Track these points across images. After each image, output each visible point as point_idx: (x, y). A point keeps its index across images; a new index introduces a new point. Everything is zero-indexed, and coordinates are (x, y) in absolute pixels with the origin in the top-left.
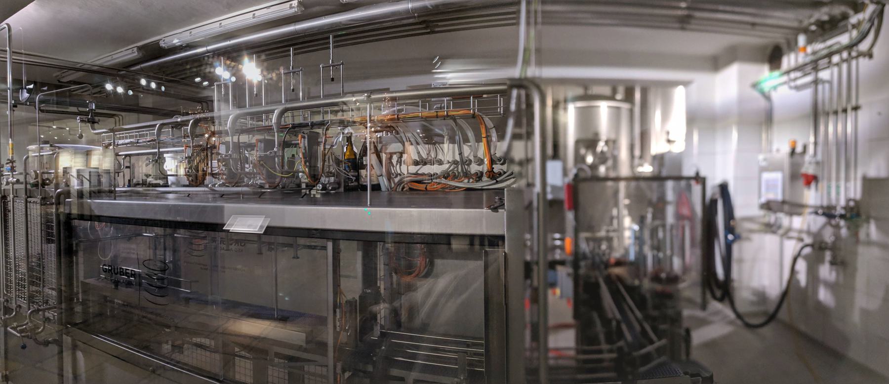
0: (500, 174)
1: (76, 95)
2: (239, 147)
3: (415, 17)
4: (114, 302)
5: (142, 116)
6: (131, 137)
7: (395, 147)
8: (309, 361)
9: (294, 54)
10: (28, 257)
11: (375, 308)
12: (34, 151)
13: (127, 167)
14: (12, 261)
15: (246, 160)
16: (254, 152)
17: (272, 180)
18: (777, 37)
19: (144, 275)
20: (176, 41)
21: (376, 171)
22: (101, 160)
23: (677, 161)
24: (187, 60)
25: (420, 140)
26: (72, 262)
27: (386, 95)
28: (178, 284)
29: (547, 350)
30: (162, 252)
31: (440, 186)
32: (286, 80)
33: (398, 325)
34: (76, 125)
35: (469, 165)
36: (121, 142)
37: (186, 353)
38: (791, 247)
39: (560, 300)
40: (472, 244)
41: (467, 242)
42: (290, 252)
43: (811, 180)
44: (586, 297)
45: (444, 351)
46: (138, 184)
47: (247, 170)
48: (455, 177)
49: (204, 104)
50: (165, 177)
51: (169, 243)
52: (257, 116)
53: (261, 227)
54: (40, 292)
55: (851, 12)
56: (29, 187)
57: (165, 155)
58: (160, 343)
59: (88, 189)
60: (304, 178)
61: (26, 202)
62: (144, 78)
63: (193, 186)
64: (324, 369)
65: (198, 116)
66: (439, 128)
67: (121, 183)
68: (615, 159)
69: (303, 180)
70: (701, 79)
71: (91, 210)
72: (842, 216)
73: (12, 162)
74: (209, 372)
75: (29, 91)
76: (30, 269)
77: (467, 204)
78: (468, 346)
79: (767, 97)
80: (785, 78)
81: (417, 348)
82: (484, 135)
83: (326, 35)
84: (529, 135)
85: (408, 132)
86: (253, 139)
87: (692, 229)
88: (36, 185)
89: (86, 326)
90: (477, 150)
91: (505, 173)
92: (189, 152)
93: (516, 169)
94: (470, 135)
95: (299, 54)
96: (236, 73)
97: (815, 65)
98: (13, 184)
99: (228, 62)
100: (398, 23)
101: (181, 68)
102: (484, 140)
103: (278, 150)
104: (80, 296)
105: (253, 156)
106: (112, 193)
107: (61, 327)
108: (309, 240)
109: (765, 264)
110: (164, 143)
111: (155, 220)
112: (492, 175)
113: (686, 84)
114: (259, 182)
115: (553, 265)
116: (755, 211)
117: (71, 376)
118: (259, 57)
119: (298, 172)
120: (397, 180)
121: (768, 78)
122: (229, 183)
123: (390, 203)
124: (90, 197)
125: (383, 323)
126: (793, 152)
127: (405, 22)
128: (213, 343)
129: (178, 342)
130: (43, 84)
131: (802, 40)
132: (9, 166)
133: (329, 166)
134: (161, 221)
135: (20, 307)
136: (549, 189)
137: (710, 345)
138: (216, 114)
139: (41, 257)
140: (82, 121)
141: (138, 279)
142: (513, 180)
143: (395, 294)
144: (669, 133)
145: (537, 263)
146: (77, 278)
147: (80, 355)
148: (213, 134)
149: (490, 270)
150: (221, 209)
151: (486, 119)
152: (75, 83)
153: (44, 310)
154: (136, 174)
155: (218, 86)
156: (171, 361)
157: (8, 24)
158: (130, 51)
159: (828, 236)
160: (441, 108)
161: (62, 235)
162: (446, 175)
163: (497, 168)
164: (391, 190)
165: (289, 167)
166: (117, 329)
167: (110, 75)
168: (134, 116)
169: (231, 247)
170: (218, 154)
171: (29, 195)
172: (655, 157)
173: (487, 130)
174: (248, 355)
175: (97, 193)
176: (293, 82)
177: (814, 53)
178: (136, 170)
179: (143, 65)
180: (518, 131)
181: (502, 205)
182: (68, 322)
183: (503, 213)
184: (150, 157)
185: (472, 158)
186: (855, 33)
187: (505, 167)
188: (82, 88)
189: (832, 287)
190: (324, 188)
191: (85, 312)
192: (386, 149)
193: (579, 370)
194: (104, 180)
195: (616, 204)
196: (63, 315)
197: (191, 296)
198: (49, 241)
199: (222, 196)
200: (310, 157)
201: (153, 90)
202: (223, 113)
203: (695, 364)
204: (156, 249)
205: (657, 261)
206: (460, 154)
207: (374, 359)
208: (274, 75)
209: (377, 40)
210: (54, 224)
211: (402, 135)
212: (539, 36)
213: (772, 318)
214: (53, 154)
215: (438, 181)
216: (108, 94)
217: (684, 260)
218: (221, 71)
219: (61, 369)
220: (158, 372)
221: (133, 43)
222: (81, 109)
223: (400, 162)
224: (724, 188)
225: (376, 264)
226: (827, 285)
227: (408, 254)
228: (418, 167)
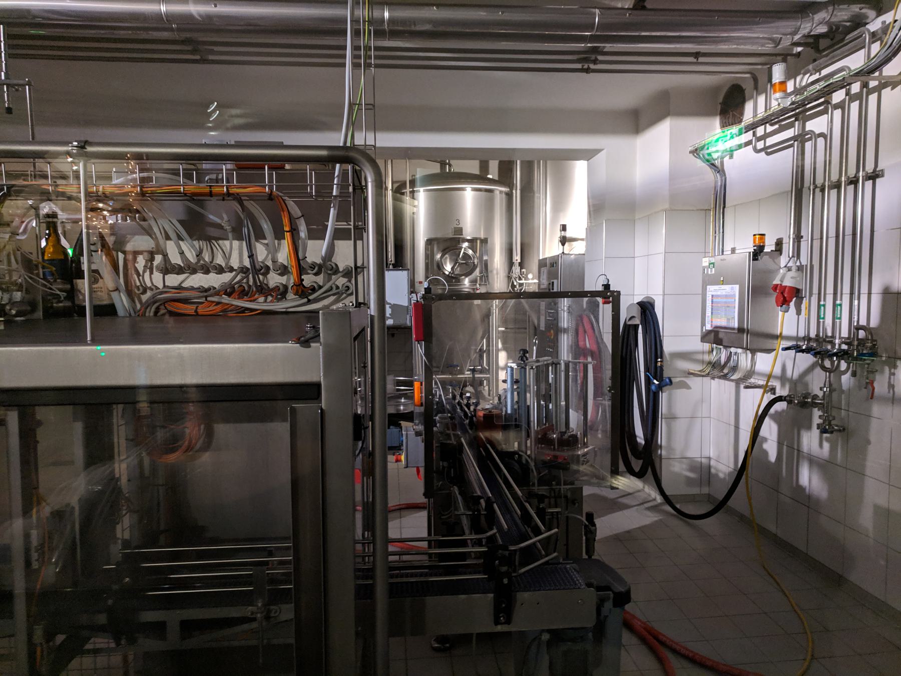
0: (314, 290)
3: (172, 30)
18: (736, 71)
23: (578, 268)
29: (388, 541)
38: (752, 401)
39: (405, 474)
43: (788, 296)
44: (442, 466)
48: (244, 294)
55: (871, 13)
66: (218, 214)
68: (486, 267)
70: (611, 146)
72: (842, 355)
79: (717, 168)
80: (749, 136)
82: (287, 228)
84: (360, 232)
87: (597, 370)
90: (276, 250)
94: (266, 226)
97: (800, 111)
100: (143, 35)
102: (287, 235)
109: (710, 424)
112: (303, 291)
113: (587, 155)
115: (395, 420)
116: (696, 345)
121: (720, 138)
123: (136, 337)
126: (758, 252)
131: (778, 72)
136: (388, 311)
137: (622, 539)
142: (332, 298)
144: (566, 223)
145: (372, 418)
151: (291, 203)
159: (817, 383)
160: (217, 181)
162: (229, 290)
163: (308, 280)
164: (137, 316)
172: (542, 263)
173: (292, 221)
177: (797, 92)
180: (343, 225)
186: (876, 48)
187: (320, 279)
189: (822, 466)
193: (433, 570)
195: (487, 333)
203: (600, 564)
205: (546, 416)
206: (251, 256)
211: (153, 223)
212: (373, 84)
213: (721, 505)
215: (215, 299)
217: (585, 413)
224: (646, 308)
226: (813, 461)
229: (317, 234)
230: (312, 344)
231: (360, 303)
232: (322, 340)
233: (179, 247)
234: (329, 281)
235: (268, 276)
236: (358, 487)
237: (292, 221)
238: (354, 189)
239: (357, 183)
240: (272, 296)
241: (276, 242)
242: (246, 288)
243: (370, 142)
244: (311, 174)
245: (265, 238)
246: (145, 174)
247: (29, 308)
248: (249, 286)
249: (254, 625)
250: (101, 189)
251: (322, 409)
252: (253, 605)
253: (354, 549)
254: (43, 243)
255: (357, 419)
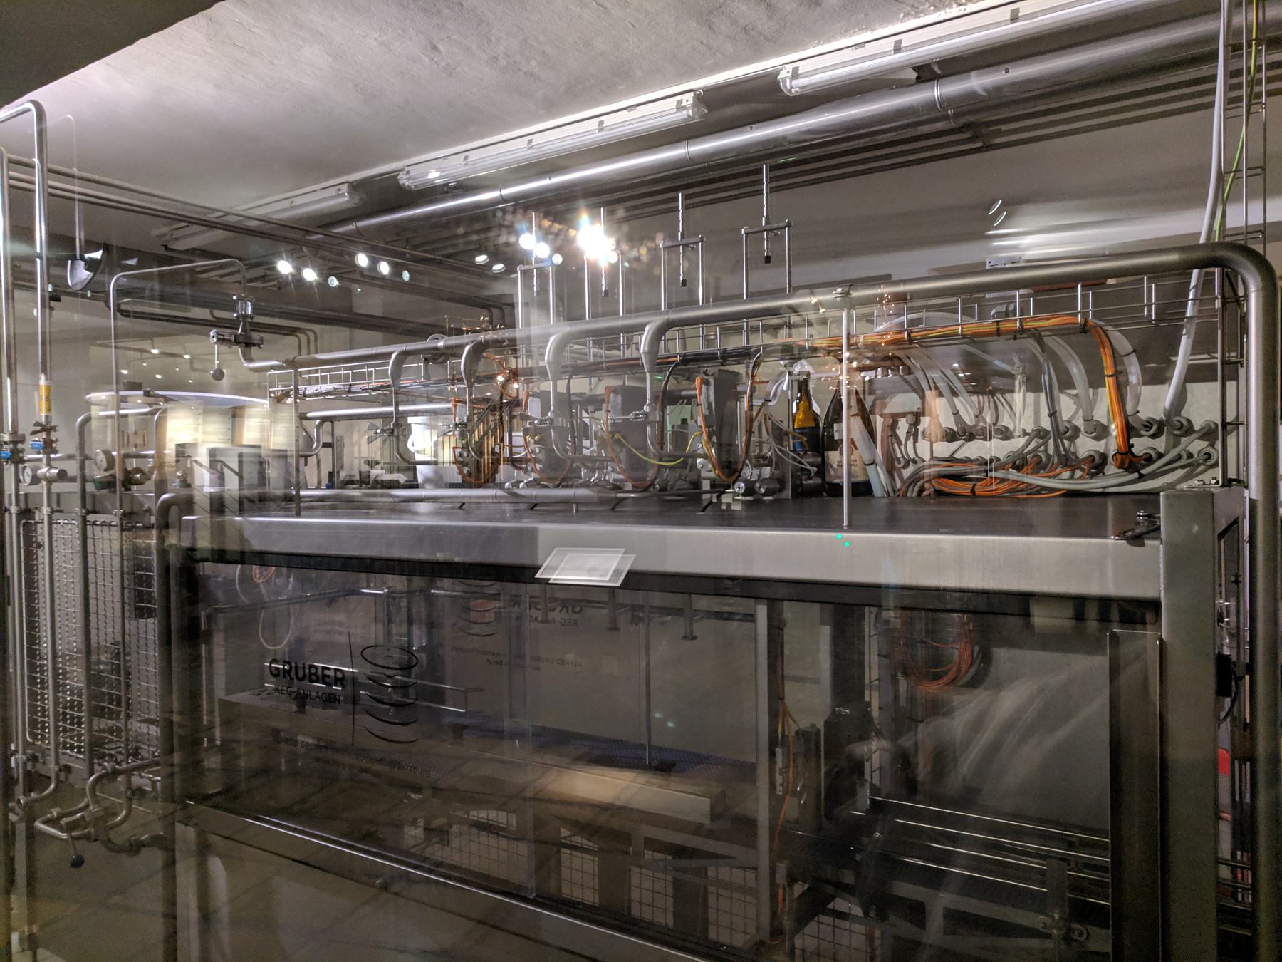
0: (1149, 460)
1: (208, 281)
2: (571, 404)
3: (947, 118)
4: (295, 743)
5: (360, 334)
6: (334, 379)
7: (903, 401)
8: (717, 856)
9: (687, 207)
10: (88, 652)
11: (860, 749)
12: (104, 405)
13: (326, 445)
14: (48, 662)
15: (585, 431)
16: (601, 414)
17: (638, 474)
19: (362, 680)
20: (434, 176)
21: (863, 453)
22: (268, 429)
24: (457, 217)
25: (958, 386)
26: (197, 657)
27: (884, 290)
28: (439, 696)
30: (404, 629)
31: (1004, 486)
32: (668, 263)
33: (911, 788)
34: (208, 349)
35: (1072, 439)
36: (311, 389)
37: (455, 843)
40: (1080, 616)
41: (1070, 612)
42: (678, 626)
45: (1014, 851)
46: (352, 482)
47: (586, 452)
48: (1040, 466)
49: (495, 312)
50: (410, 466)
51: (420, 608)
52: (607, 338)
53: (617, 572)
54: (119, 730)
56: (90, 488)
57: (411, 420)
58: (399, 825)
59: (236, 493)
60: (707, 470)
61: (85, 522)
62: (365, 251)
63: (470, 486)
64: (751, 875)
65: (482, 337)
67: (312, 478)
69: (704, 474)
71: (242, 539)
73: (47, 428)
74: (506, 882)
75: (92, 265)
76: (94, 679)
77: (1069, 527)
78: (1071, 845)
81: (953, 840)
82: (1108, 371)
83: (753, 166)
84: (1232, 369)
85: (931, 368)
86: (600, 386)
88: (109, 484)
89: (232, 798)
90: (1092, 404)
91: (1160, 456)
92: (462, 413)
93: (1197, 446)
94: (1077, 371)
95: (695, 206)
96: (563, 245)
98: (50, 481)
99: (547, 223)
100: (911, 133)
101: (446, 234)
102: (1110, 382)
103: (653, 409)
104: (217, 733)
105: (600, 422)
106: (291, 502)
107: (171, 807)
108: (717, 600)
110: (407, 394)
111: (387, 560)
112: (1129, 461)
114: (612, 477)
117: (194, 914)
118: (611, 213)
119: (694, 456)
120: (907, 473)
122: (550, 479)
123: (893, 523)
124: (241, 511)
125: (876, 781)
127: (926, 129)
128: (513, 820)
129: (437, 823)
130: (128, 252)
132: (39, 439)
133: (760, 444)
134: (400, 561)
135: (68, 769)
138: (520, 332)
139: (121, 650)
140: (222, 340)
141: (349, 689)
143: (904, 720)
145: (1250, 668)
146: (211, 692)
147: (216, 866)
148: (514, 375)
149: (1124, 677)
150: (532, 535)
151: (1116, 335)
152: (205, 253)
153: (128, 773)
154: (346, 460)
155: (524, 272)
156: (422, 861)
157: (35, 103)
158: (333, 192)
160: (1007, 314)
161: (173, 596)
162: (1019, 463)
163: (1141, 445)
164: (895, 495)
165: (676, 446)
166: (303, 801)
167: (286, 240)
168: (342, 333)
169: (551, 615)
170: (526, 418)
171: (91, 506)
173: (1117, 358)
174: (587, 844)
175: (256, 502)
176: (683, 265)
178: (346, 451)
179: (361, 224)
180: (1202, 359)
181: (1154, 531)
182: (187, 794)
183: (1155, 549)
184: (378, 422)
185: (1079, 423)
188: (222, 266)
190: (750, 490)
191: (229, 768)
192: (884, 406)
194: (273, 472)
196: (177, 779)
197: (466, 721)
198: (141, 613)
199: (533, 507)
200: (720, 425)
201: (383, 278)
202: (535, 331)
204: (390, 621)
206: (1053, 414)
207: (858, 857)
208: (643, 251)
209: (863, 172)
210: (154, 574)
211: (920, 375)
214: (152, 413)
215: (1000, 474)
216: (282, 283)
218: (531, 242)
219: (171, 901)
220: (395, 888)
221: (338, 175)
222: (220, 314)
223: (914, 434)
225: (862, 654)
227: (932, 633)
228: (956, 444)
229: (1157, 377)
230: (1147, 542)
231: (1231, 481)
232: (1163, 536)
233: (953, 406)
234: (1175, 446)
235: (1077, 441)
236: (1224, 782)
237: (1117, 358)
238: (1224, 303)
239: (1229, 293)
240: (1083, 470)
241: (1091, 391)
242: (1044, 459)
243: (1256, 219)
244: (1149, 289)
245: (1074, 388)
246: (914, 316)
247: (778, 486)
248: (1049, 457)
249: (1048, 944)
250: (861, 339)
251: (1161, 640)
252: (1046, 915)
253: (1217, 873)
254: (155, 351)
255: (1223, 663)
